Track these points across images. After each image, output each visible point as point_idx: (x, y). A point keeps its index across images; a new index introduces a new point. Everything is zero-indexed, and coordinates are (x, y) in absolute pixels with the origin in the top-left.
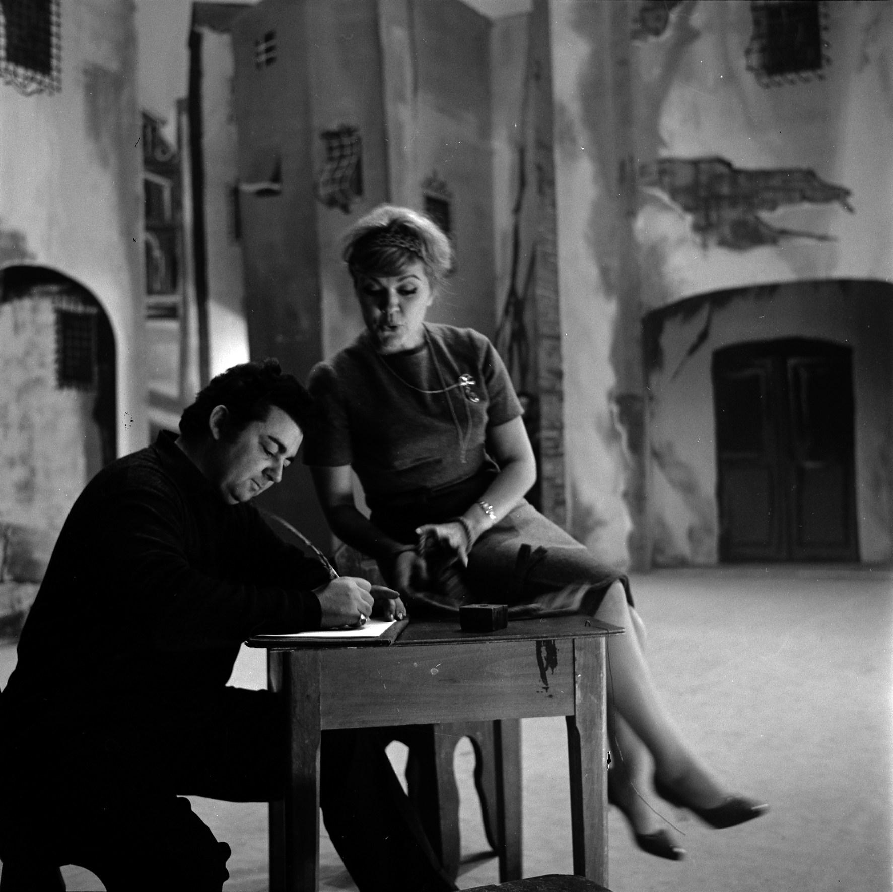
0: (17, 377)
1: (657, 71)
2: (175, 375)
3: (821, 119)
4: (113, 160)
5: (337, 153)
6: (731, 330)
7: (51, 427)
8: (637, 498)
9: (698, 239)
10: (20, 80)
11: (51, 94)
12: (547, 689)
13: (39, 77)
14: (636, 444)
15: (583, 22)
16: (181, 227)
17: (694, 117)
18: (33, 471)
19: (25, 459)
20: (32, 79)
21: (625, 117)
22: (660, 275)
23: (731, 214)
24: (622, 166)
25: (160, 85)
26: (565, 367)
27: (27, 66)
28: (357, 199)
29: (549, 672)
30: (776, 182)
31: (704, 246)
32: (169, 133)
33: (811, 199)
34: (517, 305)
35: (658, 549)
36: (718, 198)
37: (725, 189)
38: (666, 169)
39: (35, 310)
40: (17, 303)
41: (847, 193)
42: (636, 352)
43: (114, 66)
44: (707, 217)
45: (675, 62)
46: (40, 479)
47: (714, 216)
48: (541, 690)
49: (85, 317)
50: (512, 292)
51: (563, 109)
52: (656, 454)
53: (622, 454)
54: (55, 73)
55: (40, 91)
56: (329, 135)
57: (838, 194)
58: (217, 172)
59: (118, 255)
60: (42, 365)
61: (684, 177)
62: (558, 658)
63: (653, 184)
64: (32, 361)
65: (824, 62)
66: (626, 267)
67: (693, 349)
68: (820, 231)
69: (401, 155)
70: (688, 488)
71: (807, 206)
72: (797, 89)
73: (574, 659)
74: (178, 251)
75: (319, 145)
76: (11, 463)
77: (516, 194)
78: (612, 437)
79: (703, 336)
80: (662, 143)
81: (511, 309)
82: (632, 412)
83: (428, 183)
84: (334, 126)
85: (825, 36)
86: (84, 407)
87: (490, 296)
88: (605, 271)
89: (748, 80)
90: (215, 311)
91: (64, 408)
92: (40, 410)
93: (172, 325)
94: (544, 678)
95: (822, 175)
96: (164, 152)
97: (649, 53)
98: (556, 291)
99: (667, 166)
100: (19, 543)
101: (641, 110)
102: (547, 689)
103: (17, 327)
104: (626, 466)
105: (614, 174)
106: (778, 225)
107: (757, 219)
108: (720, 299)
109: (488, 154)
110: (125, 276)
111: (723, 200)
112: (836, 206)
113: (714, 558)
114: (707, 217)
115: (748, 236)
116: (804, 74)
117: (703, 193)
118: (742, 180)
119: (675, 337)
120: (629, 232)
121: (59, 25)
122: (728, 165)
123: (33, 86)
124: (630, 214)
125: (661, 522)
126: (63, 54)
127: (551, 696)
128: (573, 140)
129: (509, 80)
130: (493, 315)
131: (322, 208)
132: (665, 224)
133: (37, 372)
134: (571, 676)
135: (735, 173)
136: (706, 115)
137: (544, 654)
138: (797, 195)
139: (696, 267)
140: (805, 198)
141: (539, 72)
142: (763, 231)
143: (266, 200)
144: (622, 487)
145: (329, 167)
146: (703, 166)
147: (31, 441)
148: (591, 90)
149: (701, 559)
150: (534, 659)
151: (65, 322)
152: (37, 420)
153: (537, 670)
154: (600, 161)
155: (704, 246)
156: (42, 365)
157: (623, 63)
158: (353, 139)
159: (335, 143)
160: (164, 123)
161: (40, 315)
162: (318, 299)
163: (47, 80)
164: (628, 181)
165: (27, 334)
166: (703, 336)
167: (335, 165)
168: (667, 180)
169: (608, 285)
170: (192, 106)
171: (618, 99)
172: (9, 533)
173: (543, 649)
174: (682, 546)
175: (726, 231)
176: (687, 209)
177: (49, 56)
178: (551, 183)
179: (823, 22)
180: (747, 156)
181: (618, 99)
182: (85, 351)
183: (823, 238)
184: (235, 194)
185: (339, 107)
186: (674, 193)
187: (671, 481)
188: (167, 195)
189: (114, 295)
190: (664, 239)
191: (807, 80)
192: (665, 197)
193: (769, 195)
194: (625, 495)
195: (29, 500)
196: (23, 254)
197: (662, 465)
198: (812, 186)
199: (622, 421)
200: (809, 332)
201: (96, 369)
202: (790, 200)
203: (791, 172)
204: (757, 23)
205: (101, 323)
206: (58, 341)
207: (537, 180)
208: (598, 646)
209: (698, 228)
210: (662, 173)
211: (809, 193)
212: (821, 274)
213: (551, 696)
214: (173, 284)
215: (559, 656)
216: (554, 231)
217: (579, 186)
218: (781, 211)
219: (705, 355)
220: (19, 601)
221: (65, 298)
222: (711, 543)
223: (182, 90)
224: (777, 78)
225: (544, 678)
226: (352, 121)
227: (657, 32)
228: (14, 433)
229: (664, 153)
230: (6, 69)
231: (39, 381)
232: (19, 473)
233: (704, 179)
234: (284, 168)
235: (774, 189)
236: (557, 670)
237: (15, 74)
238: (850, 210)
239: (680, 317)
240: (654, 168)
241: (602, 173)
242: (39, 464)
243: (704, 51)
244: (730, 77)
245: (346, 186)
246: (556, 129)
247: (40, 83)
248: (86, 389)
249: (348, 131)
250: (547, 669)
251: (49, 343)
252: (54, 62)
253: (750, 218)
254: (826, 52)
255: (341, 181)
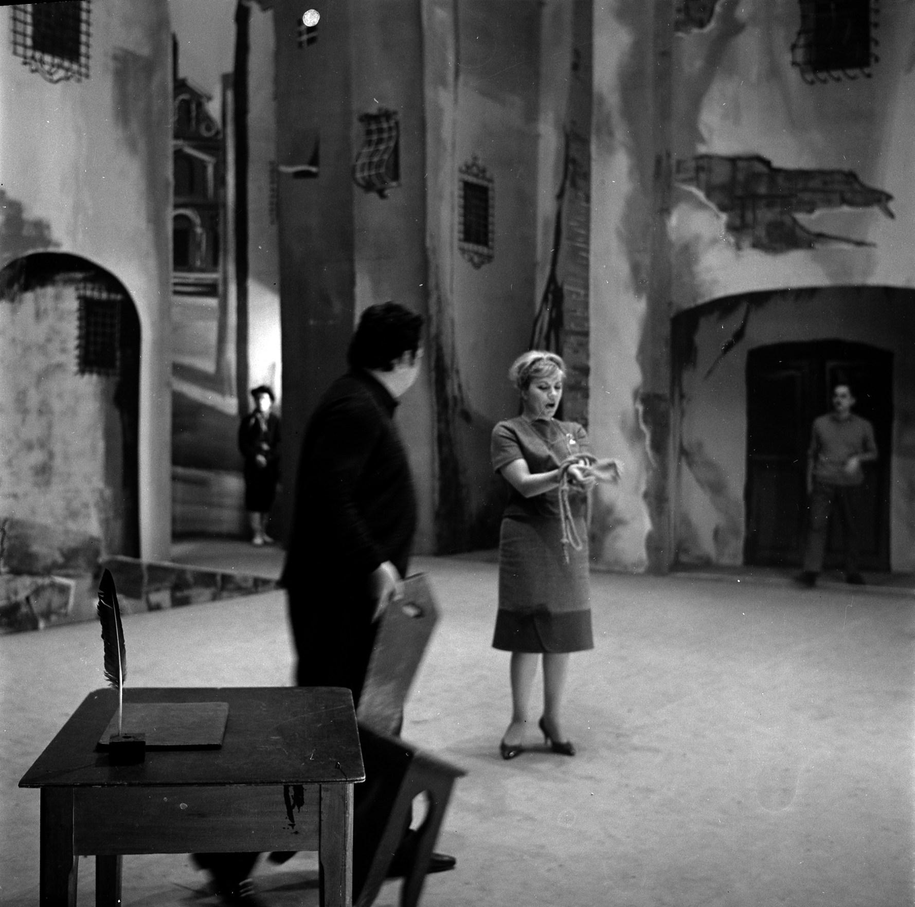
0: (37, 363)
1: (698, 64)
2: (213, 351)
3: (866, 120)
4: (142, 145)
5: (375, 137)
6: (765, 331)
7: (72, 412)
8: (657, 499)
9: (732, 240)
10: (47, 67)
11: (79, 81)
12: (293, 826)
13: (66, 64)
14: (659, 446)
15: (626, 13)
16: (224, 205)
17: (734, 114)
18: (51, 455)
19: (43, 443)
20: (60, 66)
21: (664, 113)
22: (692, 274)
23: (766, 215)
24: (658, 161)
25: (205, 61)
26: (592, 363)
27: (53, 54)
28: (394, 184)
29: (295, 810)
30: (815, 183)
31: (738, 247)
32: (214, 108)
33: (851, 203)
34: (555, 293)
35: (681, 548)
36: (755, 197)
37: (762, 190)
38: (703, 165)
39: (57, 297)
40: (39, 291)
41: (889, 197)
42: (663, 352)
43: (145, 51)
44: (743, 217)
45: (717, 56)
46: (58, 462)
47: (749, 216)
48: (286, 826)
49: (109, 304)
50: (552, 279)
51: (602, 100)
52: (684, 452)
53: (646, 453)
54: (83, 60)
55: (67, 78)
56: (367, 118)
57: (880, 198)
58: (261, 148)
59: (146, 242)
60: (63, 351)
61: (721, 174)
62: (305, 797)
63: (685, 181)
64: (54, 347)
65: (872, 60)
66: (659, 267)
67: (729, 347)
68: (856, 237)
69: (439, 140)
70: (716, 488)
71: (846, 209)
72: (843, 88)
73: (321, 799)
74: (221, 228)
75: (357, 128)
76: (29, 447)
77: (559, 183)
78: (636, 435)
79: (739, 335)
80: (702, 140)
81: (550, 296)
82: (658, 413)
83: (467, 169)
84: (373, 110)
85: (874, 33)
86: (104, 392)
87: (531, 283)
88: (636, 269)
89: (793, 75)
90: (254, 289)
91: (82, 397)
92: (60, 396)
93: (212, 302)
94: (290, 816)
95: (861, 178)
96: (208, 129)
97: (691, 45)
98: (586, 287)
99: (701, 162)
100: (16, 537)
101: (680, 104)
102: (293, 826)
103: (39, 315)
104: (648, 467)
105: (650, 171)
106: (816, 229)
107: (795, 221)
108: (757, 300)
109: (535, 138)
110: (152, 263)
111: (760, 200)
112: (876, 210)
113: (739, 560)
114: (743, 217)
115: (783, 238)
116: (851, 72)
117: (739, 192)
118: (780, 180)
119: (710, 337)
120: (663, 226)
121: (89, 11)
122: (767, 163)
123: (61, 73)
124: (665, 211)
125: (686, 521)
126: (92, 41)
127: (296, 833)
128: (611, 134)
129: (557, 64)
130: (531, 303)
131: (358, 191)
132: (698, 223)
133: (59, 358)
134: (317, 814)
135: (774, 172)
136: (743, 116)
137: (292, 793)
138: (836, 197)
139: (731, 269)
140: (844, 201)
141: (582, 62)
142: (798, 232)
143: (300, 182)
144: (643, 488)
145: (366, 150)
146: (741, 164)
147: (50, 426)
148: (631, 80)
149: (725, 561)
150: (281, 798)
151: (88, 308)
152: (57, 406)
153: (284, 808)
154: (636, 153)
155: (738, 247)
156: (63, 351)
157: (665, 54)
158: (392, 123)
159: (374, 127)
160: (210, 98)
161: (63, 304)
162: (352, 283)
163: (75, 67)
164: (662, 180)
165: (49, 320)
166: (739, 335)
167: (372, 149)
168: (703, 176)
169: (638, 283)
170: (237, 82)
171: (659, 90)
172: (6, 527)
173: (291, 789)
174: (708, 546)
175: (761, 232)
176: (723, 208)
177: (78, 43)
178: (587, 176)
179: (873, 18)
180: (786, 155)
181: (659, 90)
182: (109, 336)
183: (860, 244)
184: (275, 173)
185: (380, 92)
186: (710, 192)
187: (698, 480)
188: (210, 170)
189: (139, 280)
190: (697, 238)
191: (853, 78)
192: (701, 195)
193: (806, 196)
194: (646, 495)
195: (48, 483)
196: (48, 242)
197: (690, 464)
198: (854, 189)
199: (645, 422)
200: (850, 335)
201: (118, 354)
202: (829, 203)
203: (831, 173)
204: (804, 17)
205: (128, 307)
206: (80, 328)
207: (575, 174)
208: (345, 789)
209: (731, 228)
210: (699, 169)
211: (848, 196)
212: (857, 280)
213: (296, 833)
214: (214, 263)
215: (307, 796)
216: (586, 225)
217: (614, 180)
218: (817, 213)
219: (738, 358)
220: (16, 593)
221: (89, 286)
222: (737, 546)
223: (228, 66)
224: (822, 75)
225: (290, 816)
226: (391, 106)
227: (701, 24)
228: (32, 417)
229: (702, 149)
230: (33, 58)
231: (60, 366)
232: (37, 457)
233: (741, 177)
234: (322, 153)
235: (814, 191)
236: (303, 808)
237: (42, 62)
238: (891, 215)
239: (716, 314)
240: (692, 164)
241: (637, 168)
242: (57, 448)
243: (748, 46)
244: (773, 72)
245: (382, 170)
246: (594, 120)
247: (67, 70)
248: (107, 375)
249: (387, 115)
250: (293, 807)
251: (71, 329)
252: (83, 49)
253: (787, 220)
254: (874, 50)
255: (379, 165)
